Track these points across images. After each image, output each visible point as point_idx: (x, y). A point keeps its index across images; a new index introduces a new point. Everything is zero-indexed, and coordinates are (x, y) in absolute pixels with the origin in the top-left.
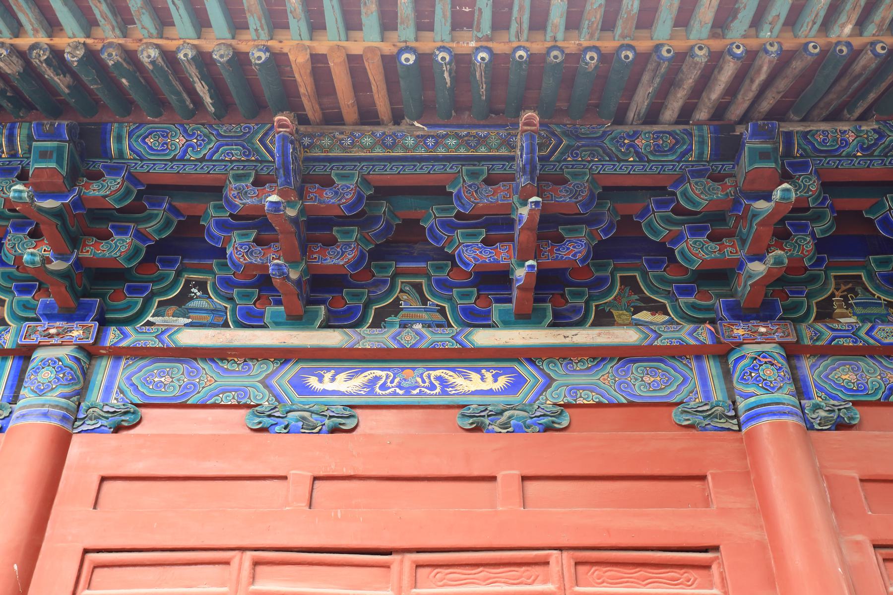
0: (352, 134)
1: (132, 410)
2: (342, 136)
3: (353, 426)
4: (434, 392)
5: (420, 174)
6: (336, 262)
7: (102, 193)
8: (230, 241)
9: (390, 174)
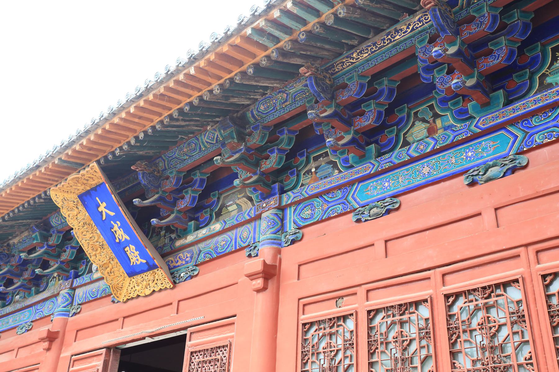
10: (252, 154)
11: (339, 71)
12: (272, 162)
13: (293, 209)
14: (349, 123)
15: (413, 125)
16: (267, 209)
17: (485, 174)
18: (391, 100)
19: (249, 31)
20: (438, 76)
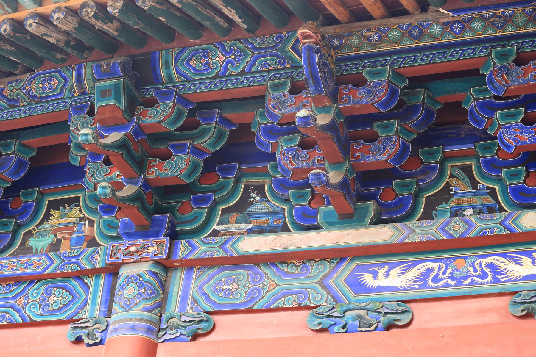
0: (379, 30)
1: (205, 319)
2: (370, 33)
3: (407, 321)
4: (486, 280)
5: (450, 61)
6: (379, 158)
7: (157, 119)
8: (278, 146)
9: (420, 65)
20: (284, 146)
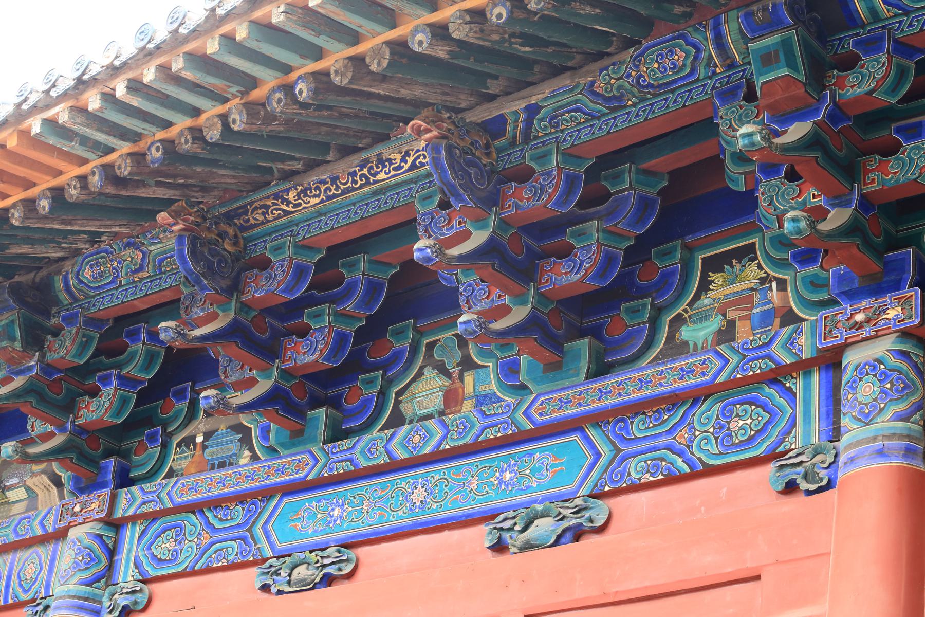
7: (865, 88)
10: (60, 379)
11: (256, 225)
12: (101, 408)
13: (139, 528)
14: (267, 351)
15: (420, 374)
16: (81, 520)
17: (524, 530)
18: (371, 309)
19: (35, 126)
